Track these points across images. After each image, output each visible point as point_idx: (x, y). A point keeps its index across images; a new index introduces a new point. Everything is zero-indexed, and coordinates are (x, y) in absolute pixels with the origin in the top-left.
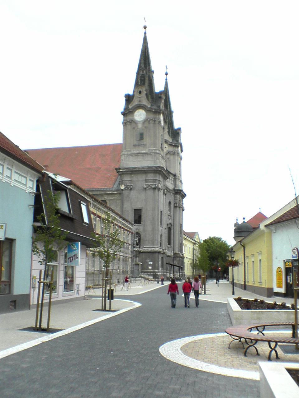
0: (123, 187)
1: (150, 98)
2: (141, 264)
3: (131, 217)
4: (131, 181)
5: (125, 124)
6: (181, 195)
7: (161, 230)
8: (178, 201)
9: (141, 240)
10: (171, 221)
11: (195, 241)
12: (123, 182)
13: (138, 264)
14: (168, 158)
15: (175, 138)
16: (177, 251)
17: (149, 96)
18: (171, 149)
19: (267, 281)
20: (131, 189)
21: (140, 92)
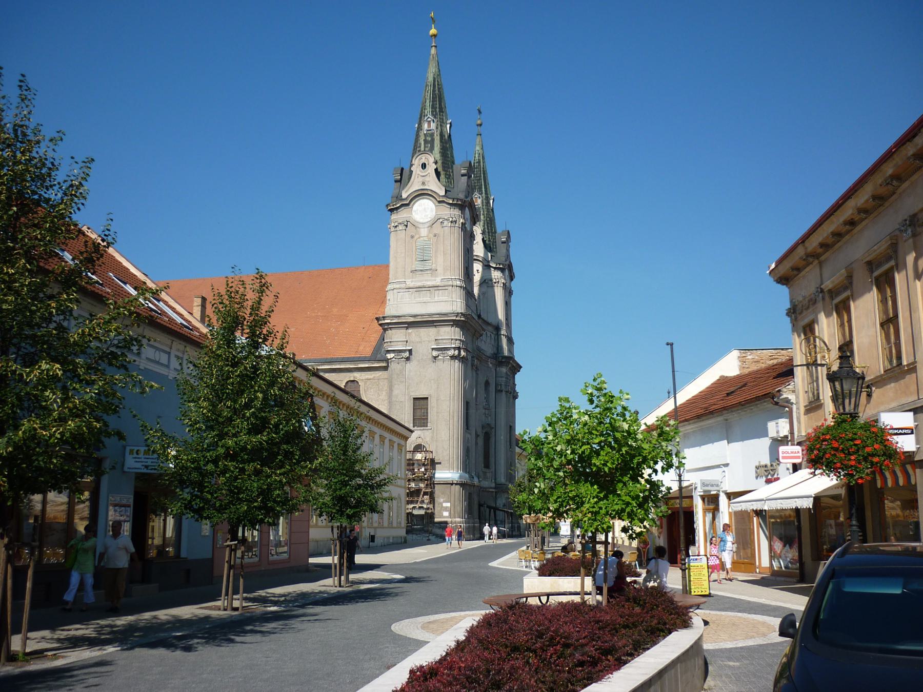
16: (502, 479)
21: (424, 166)
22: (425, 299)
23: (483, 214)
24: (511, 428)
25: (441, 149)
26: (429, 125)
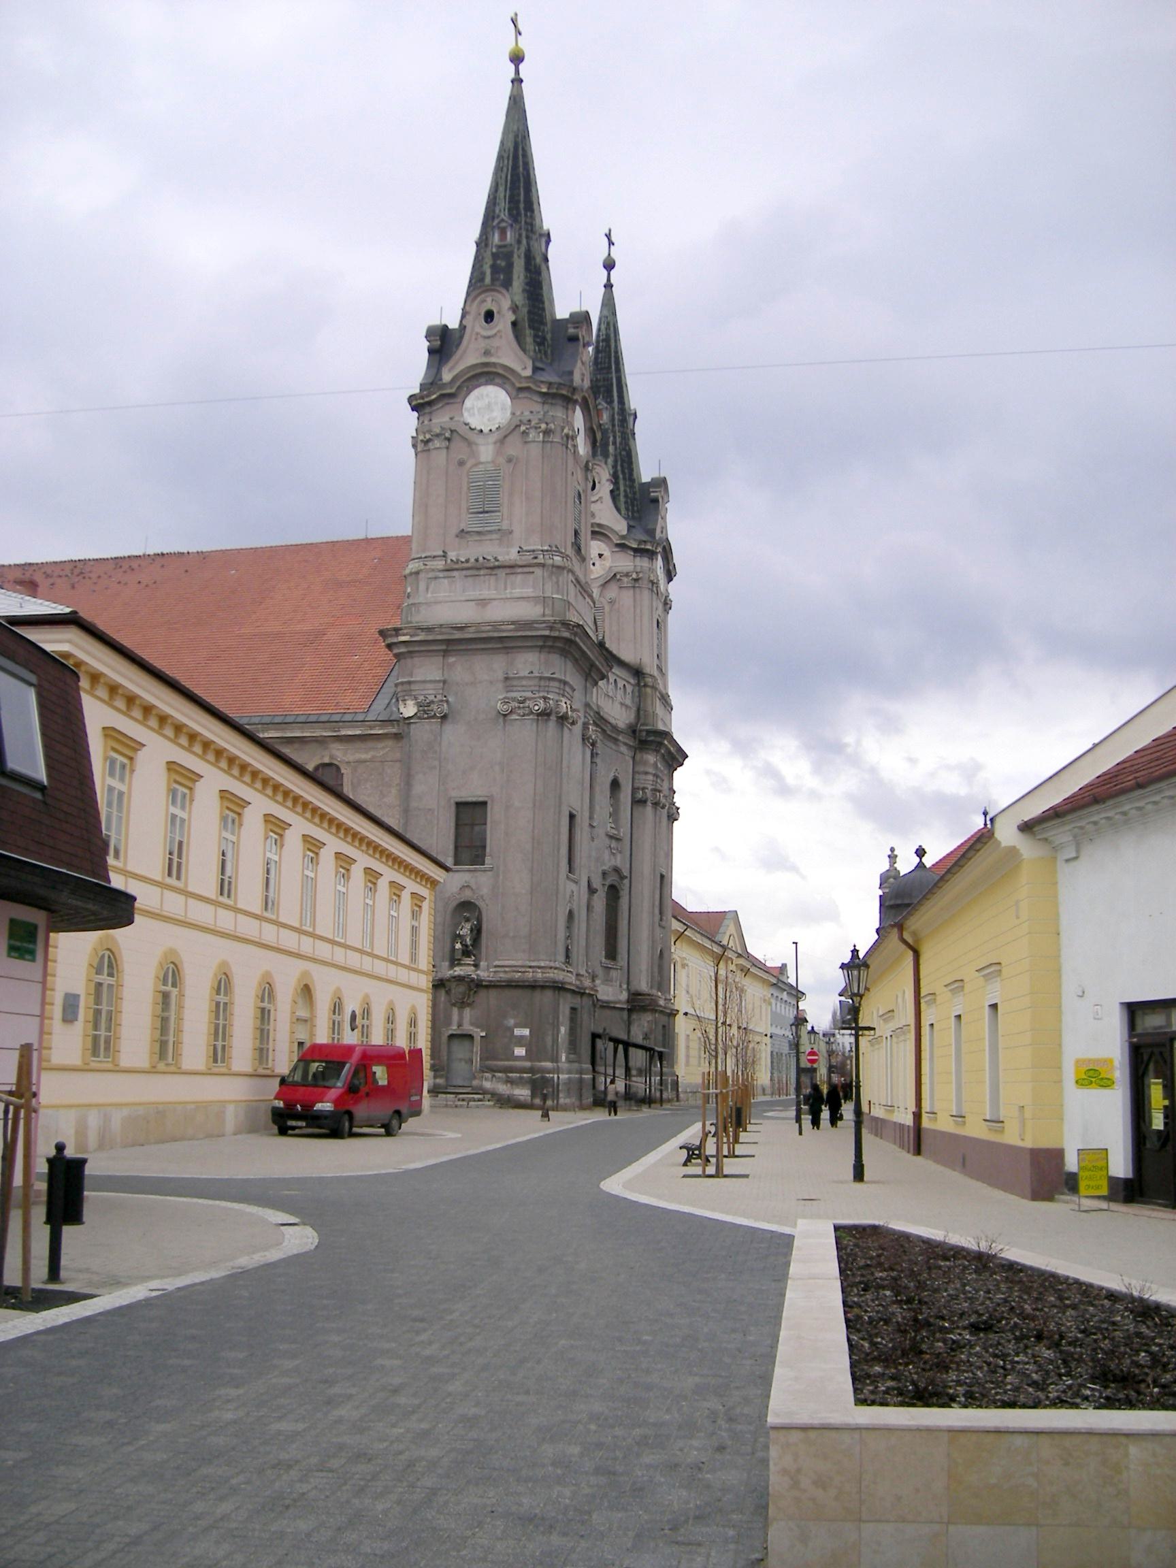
0: (409, 710)
1: (529, 340)
2: (483, 1034)
3: (441, 838)
4: (444, 682)
5: (422, 444)
6: (663, 756)
7: (572, 896)
8: (651, 777)
9: (484, 935)
10: (620, 861)
11: (725, 948)
12: (413, 687)
13: (470, 1037)
14: (612, 602)
15: (640, 519)
16: (643, 985)
17: (528, 332)
18: (626, 563)
19: (1028, 1114)
20: (444, 717)
21: (489, 316)
22: (486, 593)
23: (614, 443)
24: (664, 880)
25: (527, 284)
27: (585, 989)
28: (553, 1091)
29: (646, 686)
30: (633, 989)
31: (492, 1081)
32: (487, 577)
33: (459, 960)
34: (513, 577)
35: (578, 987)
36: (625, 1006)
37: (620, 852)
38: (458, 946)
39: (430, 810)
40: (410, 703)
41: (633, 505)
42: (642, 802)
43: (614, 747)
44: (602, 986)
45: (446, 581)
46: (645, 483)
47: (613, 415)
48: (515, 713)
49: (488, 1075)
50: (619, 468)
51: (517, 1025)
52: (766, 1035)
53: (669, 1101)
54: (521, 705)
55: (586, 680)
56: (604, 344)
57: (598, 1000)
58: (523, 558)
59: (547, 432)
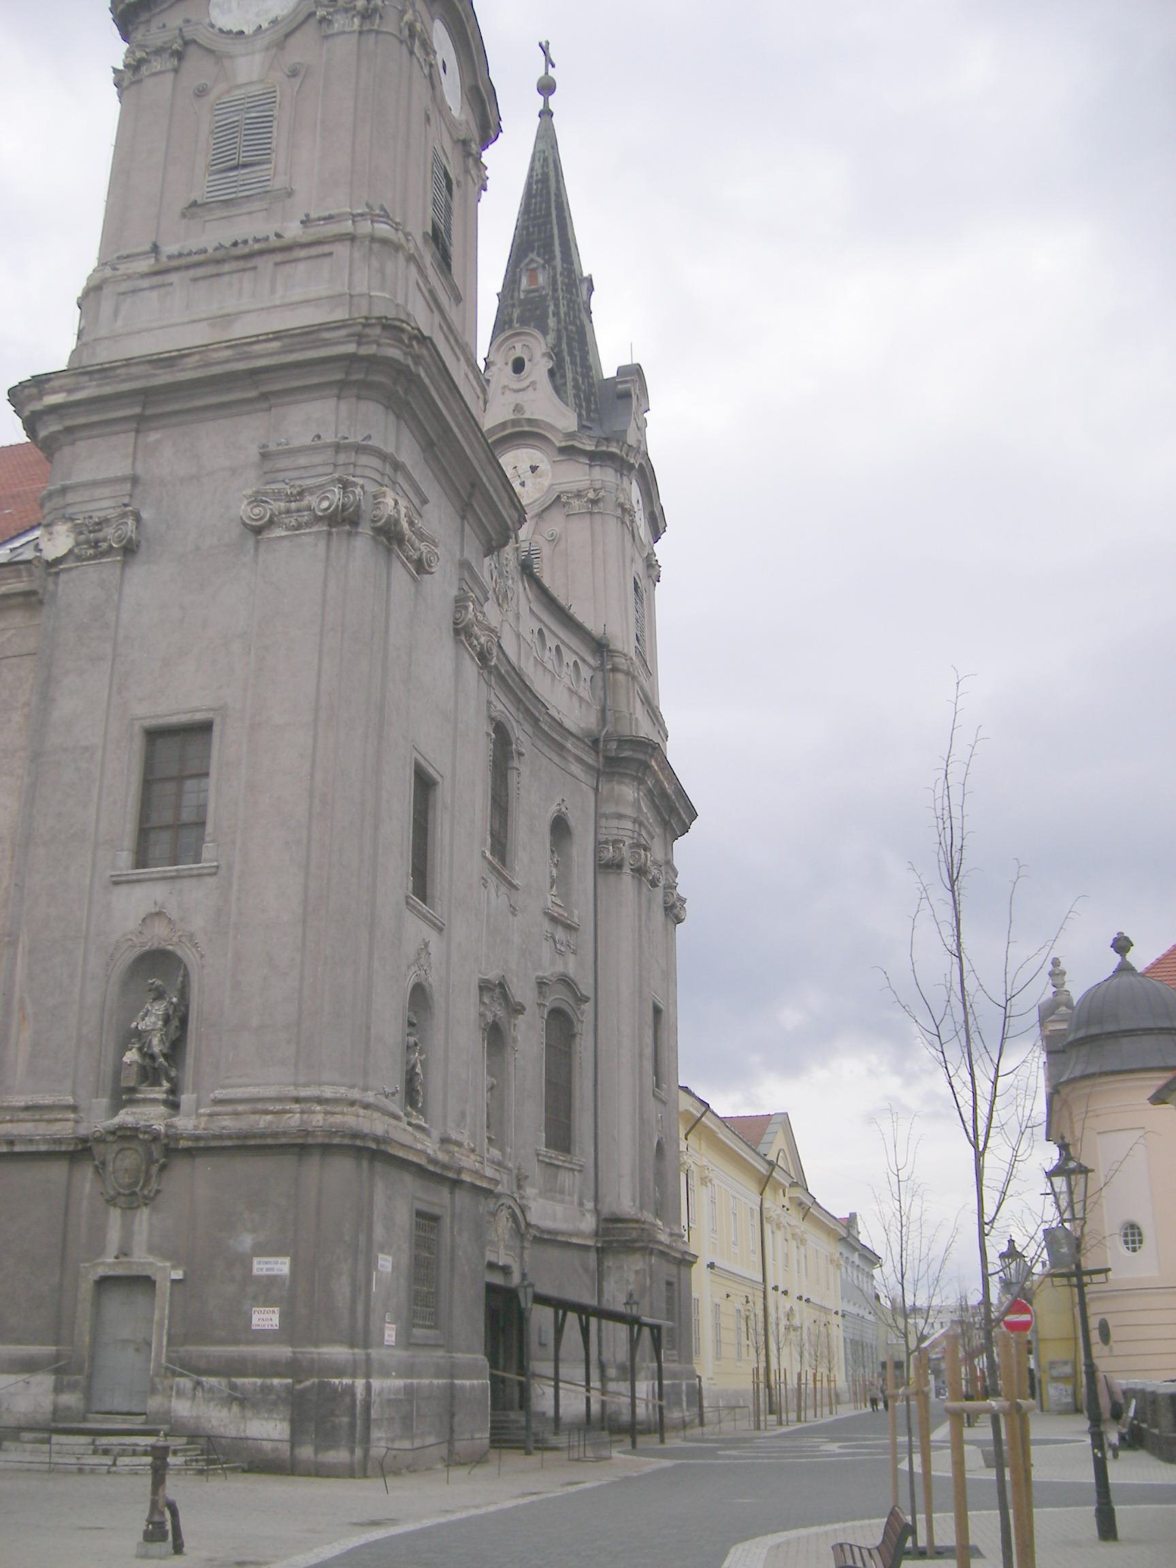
0: (58, 543)
2: (178, 1274)
4: (135, 480)
6: (650, 792)
8: (629, 825)
11: (772, 1165)
12: (71, 497)
13: (145, 1283)
16: (626, 1205)
18: (576, 476)
20: (129, 550)
22: (231, 305)
26: (533, 278)
27: (459, 1170)
28: (352, 1425)
29: (615, 670)
30: (606, 1211)
31: (194, 1398)
32: (235, 276)
33: (132, 1090)
34: (288, 269)
35: (445, 1166)
36: (590, 1242)
37: (574, 953)
38: (131, 1056)
39: (86, 749)
40: (62, 529)
41: (588, 401)
42: (615, 866)
43: (556, 759)
44: (541, 1201)
45: (154, 294)
46: (607, 379)
47: (554, 277)
48: (280, 525)
49: (185, 1383)
50: (564, 346)
51: (262, 1250)
52: (836, 1313)
53: (684, 1425)
54: (293, 505)
55: (463, 518)
56: (540, 186)
57: (528, 1225)
58: (312, 230)
59: (367, 15)
